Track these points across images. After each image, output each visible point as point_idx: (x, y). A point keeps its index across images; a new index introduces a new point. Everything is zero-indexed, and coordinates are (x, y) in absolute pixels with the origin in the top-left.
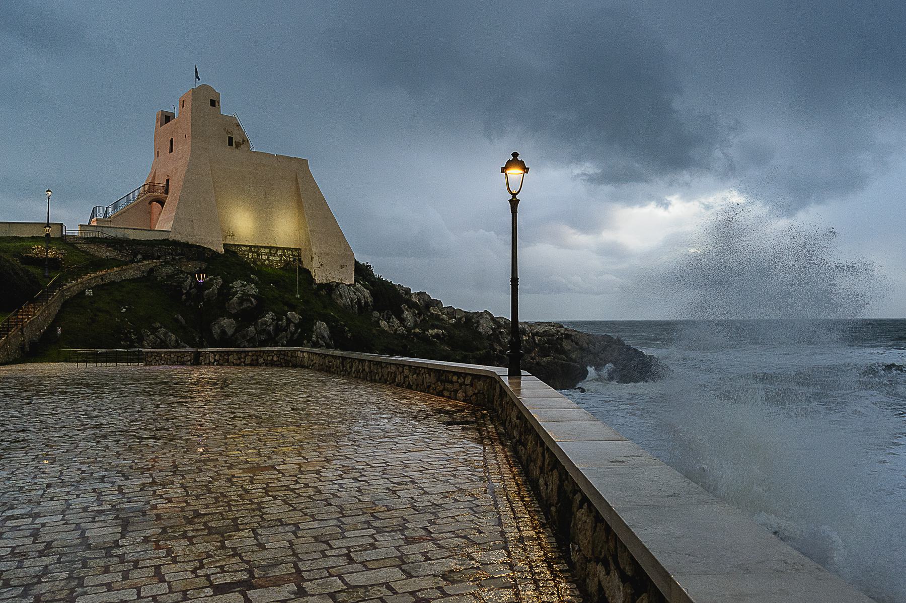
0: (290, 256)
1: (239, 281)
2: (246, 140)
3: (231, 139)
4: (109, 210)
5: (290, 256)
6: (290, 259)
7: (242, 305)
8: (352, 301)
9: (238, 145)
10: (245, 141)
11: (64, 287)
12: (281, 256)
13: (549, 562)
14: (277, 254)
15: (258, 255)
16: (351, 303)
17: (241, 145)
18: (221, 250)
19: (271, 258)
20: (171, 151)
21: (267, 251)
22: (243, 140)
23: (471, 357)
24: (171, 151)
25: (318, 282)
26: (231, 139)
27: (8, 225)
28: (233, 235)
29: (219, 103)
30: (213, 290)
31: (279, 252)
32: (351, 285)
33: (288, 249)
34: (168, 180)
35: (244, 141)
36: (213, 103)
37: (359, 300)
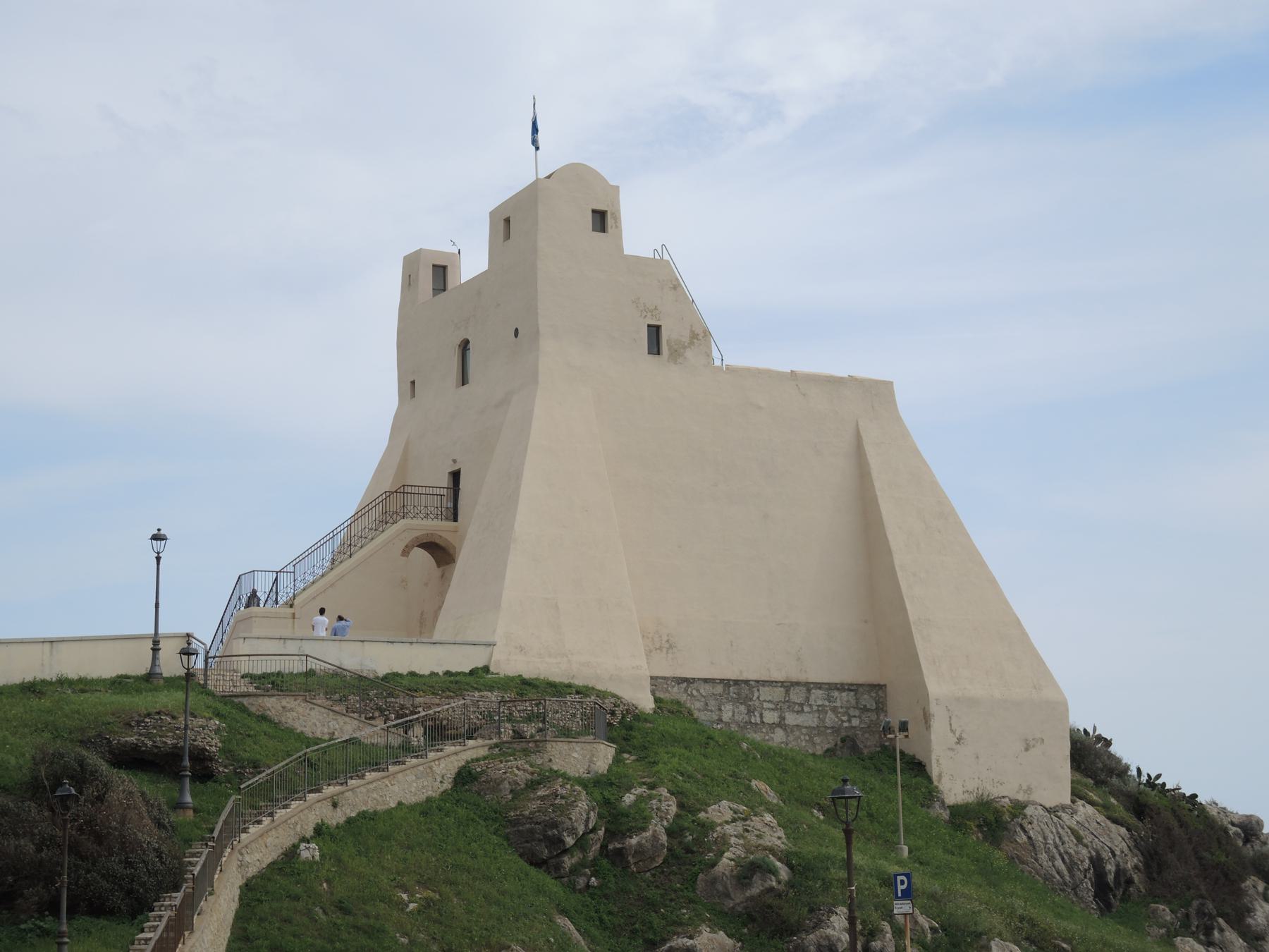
0: (852, 712)
1: (724, 803)
2: (699, 331)
3: (655, 332)
4: (285, 580)
5: (852, 712)
6: (849, 721)
7: (749, 885)
8: (1071, 867)
9: (677, 354)
10: (700, 337)
11: (243, 836)
12: (821, 710)
13: (1080, 791)
14: (811, 706)
15: (750, 711)
16: (1072, 875)
17: (685, 348)
18: (646, 703)
19: (791, 719)
20: (464, 380)
21: (778, 693)
22: (692, 332)
23: (1009, 820)
24: (464, 380)
25: (951, 800)
26: (655, 332)
27: (47, 646)
28: (671, 647)
29: (617, 219)
30: (655, 837)
31: (817, 696)
32: (1063, 808)
33: (841, 687)
34: (456, 476)
35: (694, 336)
36: (601, 220)
37: (1097, 862)
